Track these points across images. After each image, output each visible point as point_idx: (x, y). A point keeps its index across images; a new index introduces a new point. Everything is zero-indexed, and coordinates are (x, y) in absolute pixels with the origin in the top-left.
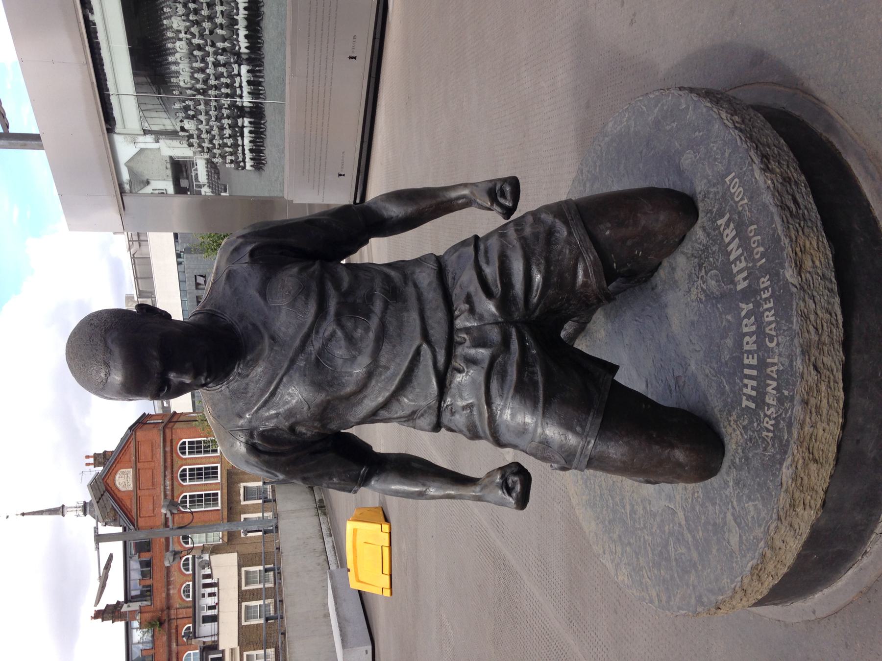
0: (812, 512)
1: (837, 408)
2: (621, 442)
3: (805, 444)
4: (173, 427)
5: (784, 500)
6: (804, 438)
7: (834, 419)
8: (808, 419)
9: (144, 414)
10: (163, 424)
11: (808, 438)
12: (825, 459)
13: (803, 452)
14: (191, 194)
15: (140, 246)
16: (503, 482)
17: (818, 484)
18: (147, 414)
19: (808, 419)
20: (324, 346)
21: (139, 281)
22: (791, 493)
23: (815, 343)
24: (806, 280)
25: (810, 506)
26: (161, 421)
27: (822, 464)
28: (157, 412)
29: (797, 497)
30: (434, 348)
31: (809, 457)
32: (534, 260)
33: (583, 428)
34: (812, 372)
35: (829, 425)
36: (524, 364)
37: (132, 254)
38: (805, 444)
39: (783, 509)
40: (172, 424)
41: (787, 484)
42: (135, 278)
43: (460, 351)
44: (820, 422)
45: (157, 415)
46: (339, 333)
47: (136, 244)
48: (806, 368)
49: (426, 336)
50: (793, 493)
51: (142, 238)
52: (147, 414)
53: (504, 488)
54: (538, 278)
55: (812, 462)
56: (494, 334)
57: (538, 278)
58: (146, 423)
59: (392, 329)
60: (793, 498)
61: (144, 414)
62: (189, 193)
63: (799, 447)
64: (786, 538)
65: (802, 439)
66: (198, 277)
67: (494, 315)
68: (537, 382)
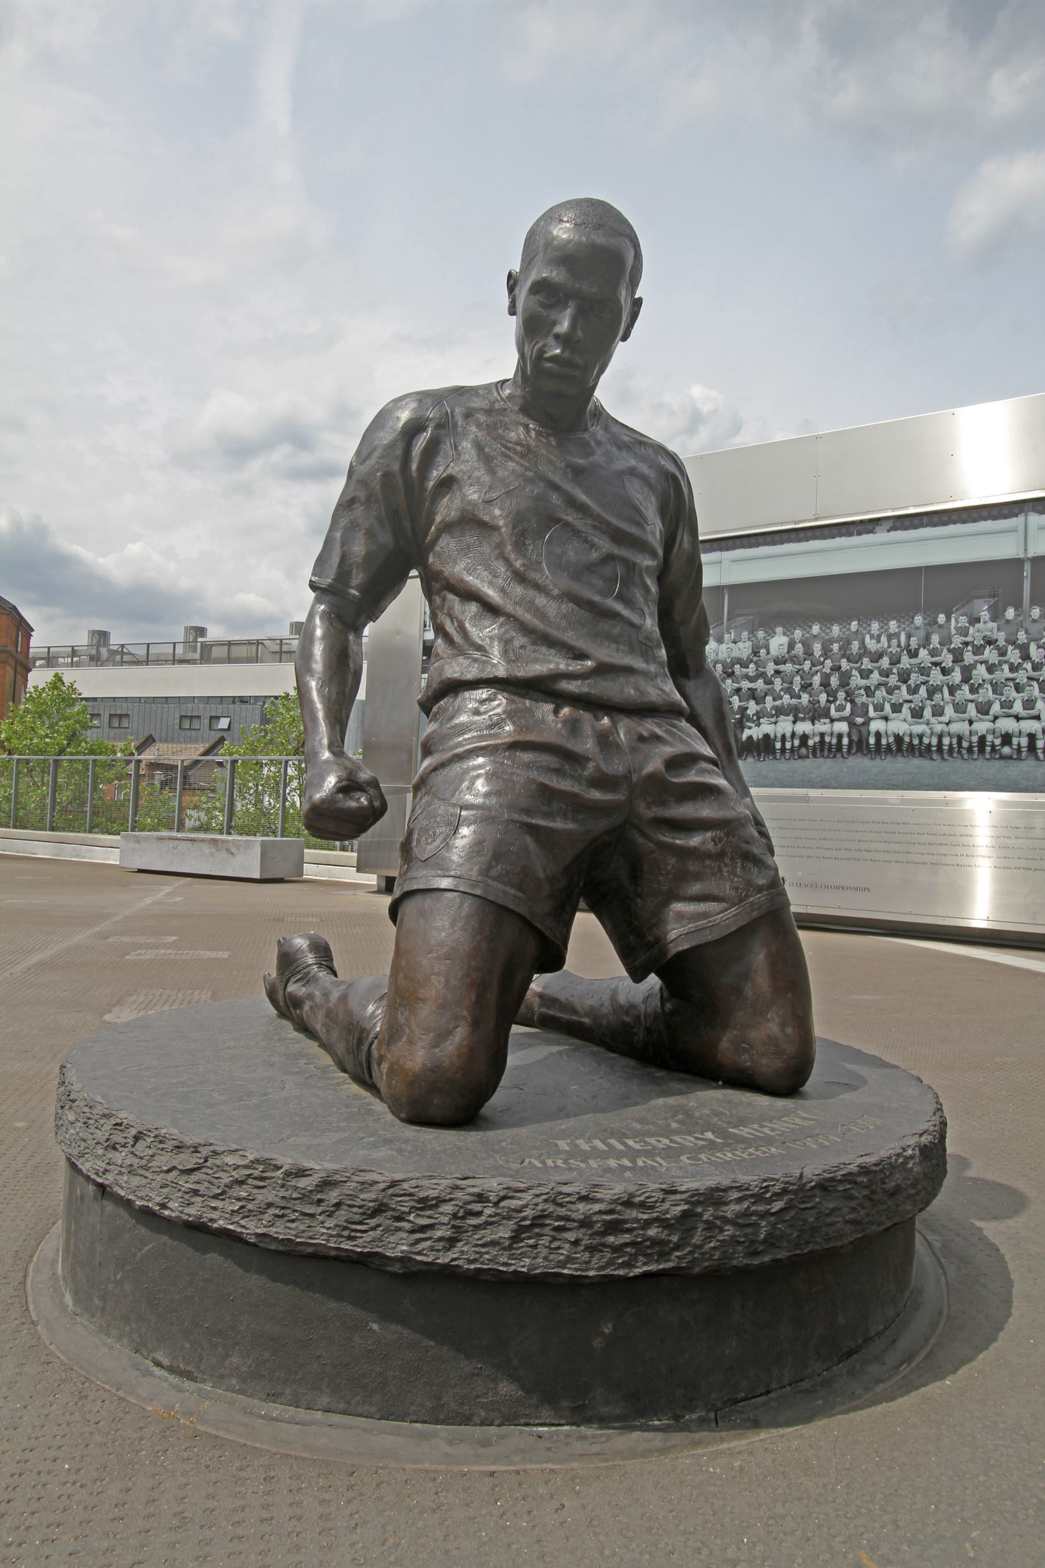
0: (405, 1248)
1: (615, 1264)
2: (479, 937)
3: (550, 1207)
4: (9, 664)
5: (436, 1187)
6: (561, 1205)
7: (595, 1260)
8: (597, 1207)
9: (33, 630)
10: (14, 652)
11: (562, 1211)
12: (519, 1252)
13: (536, 1205)
14: (423, 660)
15: (274, 652)
16: (357, 783)
17: (465, 1249)
18: (32, 633)
19: (597, 1207)
20: (576, 533)
21: (226, 648)
22: (452, 1196)
23: (723, 1211)
24: (809, 1197)
25: (418, 1241)
26: (19, 650)
27: (510, 1248)
28: (31, 650)
29: (441, 1210)
30: (588, 678)
31: (524, 1219)
32: (719, 833)
33: (497, 878)
34: (679, 1208)
35: (583, 1251)
36: (576, 806)
37: (264, 642)
38: (550, 1207)
39: (417, 1187)
40: (14, 665)
41: (469, 1186)
42: (229, 641)
43: (586, 716)
44: (589, 1232)
45: (28, 648)
46: (595, 555)
47: (277, 648)
48: (684, 1196)
49: (603, 670)
50: (451, 1200)
51: (284, 656)
52: (32, 633)
53: (349, 783)
54: (695, 841)
55: (515, 1227)
56: (616, 767)
57: (695, 841)
58: (18, 630)
59: (605, 626)
60: (440, 1201)
61: (33, 630)
62: (425, 658)
63: (545, 1197)
64: (345, 1207)
65: (560, 1201)
66: (229, 719)
67: (641, 769)
68: (553, 819)
